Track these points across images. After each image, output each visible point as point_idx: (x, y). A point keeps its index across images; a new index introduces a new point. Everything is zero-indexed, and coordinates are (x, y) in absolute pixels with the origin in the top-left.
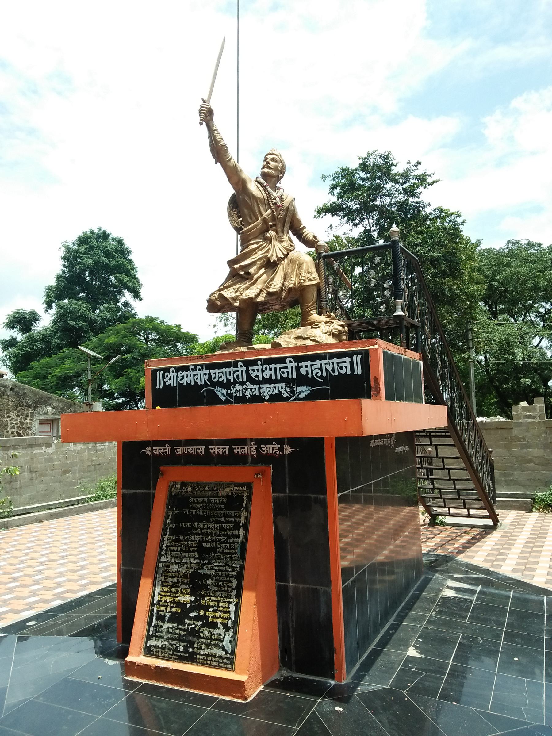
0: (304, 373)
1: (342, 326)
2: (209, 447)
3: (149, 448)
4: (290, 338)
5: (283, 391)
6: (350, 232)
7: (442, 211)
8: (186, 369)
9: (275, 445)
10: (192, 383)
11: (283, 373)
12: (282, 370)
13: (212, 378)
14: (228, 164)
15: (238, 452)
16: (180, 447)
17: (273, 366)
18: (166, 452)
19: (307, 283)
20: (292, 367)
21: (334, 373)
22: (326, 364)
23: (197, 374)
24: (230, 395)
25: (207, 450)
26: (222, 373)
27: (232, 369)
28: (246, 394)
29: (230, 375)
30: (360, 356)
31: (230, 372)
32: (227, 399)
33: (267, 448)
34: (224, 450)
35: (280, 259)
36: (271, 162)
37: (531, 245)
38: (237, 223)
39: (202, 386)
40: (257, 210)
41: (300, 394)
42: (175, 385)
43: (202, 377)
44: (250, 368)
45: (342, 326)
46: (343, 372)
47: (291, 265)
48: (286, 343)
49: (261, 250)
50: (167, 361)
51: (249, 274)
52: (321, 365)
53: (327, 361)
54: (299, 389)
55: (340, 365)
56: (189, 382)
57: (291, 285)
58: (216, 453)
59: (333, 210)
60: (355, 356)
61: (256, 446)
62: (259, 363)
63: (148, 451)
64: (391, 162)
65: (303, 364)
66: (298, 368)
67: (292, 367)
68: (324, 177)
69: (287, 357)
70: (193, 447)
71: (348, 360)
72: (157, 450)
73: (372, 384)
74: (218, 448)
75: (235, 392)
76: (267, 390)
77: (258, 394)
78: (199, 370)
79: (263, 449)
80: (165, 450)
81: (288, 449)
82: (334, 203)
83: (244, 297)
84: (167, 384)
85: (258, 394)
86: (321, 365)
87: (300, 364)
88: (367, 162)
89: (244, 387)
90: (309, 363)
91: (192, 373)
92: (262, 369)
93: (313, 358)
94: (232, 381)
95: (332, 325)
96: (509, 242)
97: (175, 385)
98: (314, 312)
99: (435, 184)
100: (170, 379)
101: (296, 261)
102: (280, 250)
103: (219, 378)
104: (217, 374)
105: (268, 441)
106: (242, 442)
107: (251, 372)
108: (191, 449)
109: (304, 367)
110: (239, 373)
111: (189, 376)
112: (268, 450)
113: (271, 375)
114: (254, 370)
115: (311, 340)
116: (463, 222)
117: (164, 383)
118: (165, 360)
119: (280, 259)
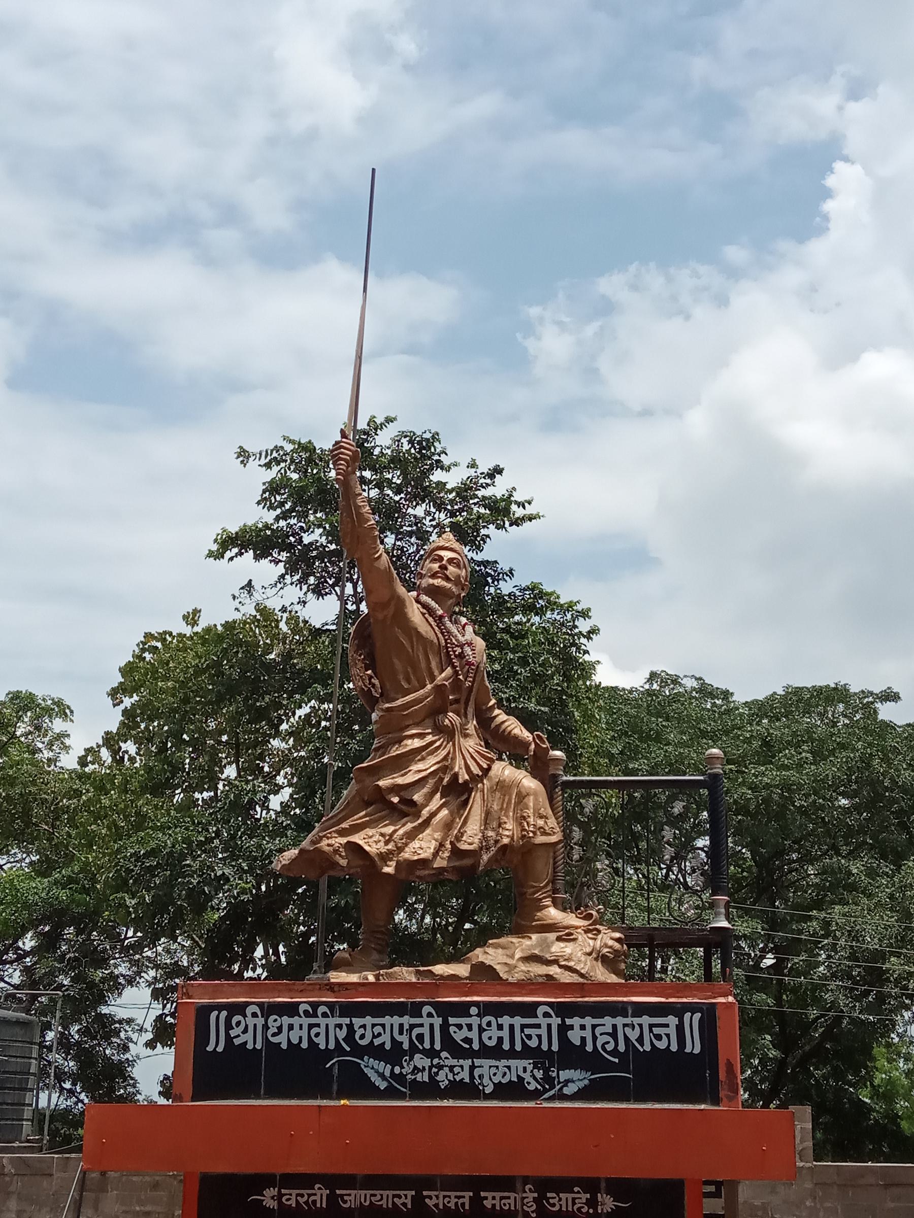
0: (577, 1042)
1: (618, 940)
2: (425, 1193)
3: (271, 1192)
4: (512, 956)
5: (527, 1077)
6: (298, 607)
7: (542, 595)
8: (291, 1010)
9: (578, 1192)
10: (304, 1045)
11: (529, 1037)
12: (527, 1031)
13: (357, 1037)
14: (376, 564)
15: (494, 1205)
16: (353, 1192)
17: (506, 1020)
18: (314, 1202)
19: (540, 839)
20: (549, 1026)
21: (642, 1045)
22: (625, 1025)
23: (318, 1025)
24: (400, 1078)
25: (418, 1200)
26: (383, 1026)
27: (407, 1020)
28: (438, 1078)
29: (401, 1033)
30: (698, 1016)
31: (401, 1026)
32: (390, 1087)
33: (560, 1200)
34: (461, 1201)
35: (476, 779)
36: (450, 568)
37: (706, 691)
38: (363, 680)
39: (328, 1054)
40: (423, 665)
41: (566, 1085)
42: (258, 1046)
43: (329, 1032)
44: (452, 1020)
45: (618, 940)
46: (662, 1045)
47: (498, 794)
48: (507, 969)
49: (432, 753)
50: (238, 989)
51: (413, 803)
52: (614, 1027)
53: (628, 1020)
54: (564, 1075)
55: (656, 1030)
56: (295, 1041)
57: (506, 841)
58: (441, 1207)
59: (257, 541)
60: (687, 1015)
61: (536, 1195)
62: (474, 1010)
63: (269, 1198)
64: (436, 457)
65: (576, 1021)
66: (564, 1029)
67: (549, 1026)
68: (243, 455)
69: (539, 1004)
70: (385, 1193)
71: (672, 1020)
72: (291, 1197)
73: (722, 1075)
74: (445, 1197)
75: (413, 1073)
76: (490, 1073)
77: (467, 1080)
78: (325, 1015)
79: (551, 1201)
80: (312, 1198)
81: (607, 1203)
82: (267, 526)
83: (407, 855)
84: (237, 1042)
85: (467, 1080)
86: (614, 1027)
87: (568, 1021)
88: (366, 441)
89: (436, 1061)
90: (588, 1021)
91: (306, 1021)
92: (480, 1026)
93: (598, 1010)
94: (406, 1046)
95: (600, 937)
96: (653, 676)
97: (258, 1046)
98: (548, 902)
99: (527, 524)
100: (245, 1031)
101: (510, 787)
102: (472, 757)
103: (374, 1037)
104: (369, 1028)
105: (563, 1185)
106: (504, 1183)
107: (452, 1029)
108: (379, 1197)
109: (577, 1027)
110: (426, 1031)
111: (296, 1027)
112: (563, 1203)
113: (500, 1039)
114: (460, 1027)
115: (561, 967)
116: (594, 631)
117: (229, 1039)
118: (233, 985)
119: (476, 779)
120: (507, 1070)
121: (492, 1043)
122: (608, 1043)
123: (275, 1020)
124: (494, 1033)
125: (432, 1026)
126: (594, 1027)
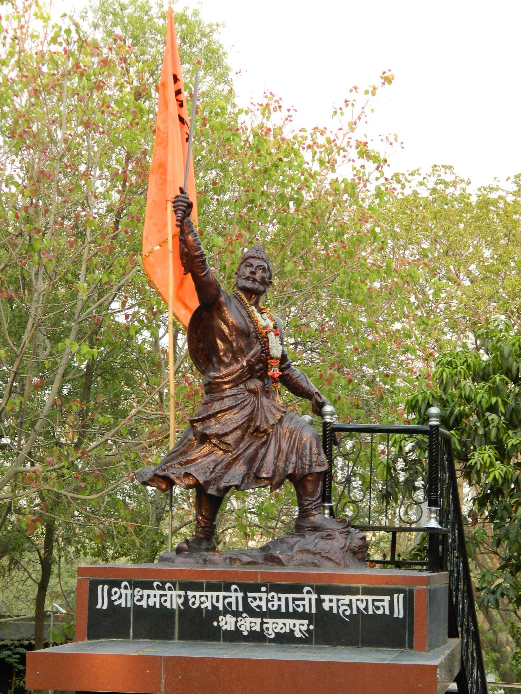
10: (158, 606)
22: (357, 600)
23: (166, 595)
27: (221, 594)
29: (218, 601)
31: (218, 597)
44: (250, 594)
52: (351, 601)
55: (377, 604)
60: (396, 596)
65: (327, 597)
66: (319, 602)
71: (387, 598)
76: (274, 626)
78: (170, 589)
84: (116, 603)
86: (351, 601)
87: (322, 597)
91: (158, 593)
92: (267, 598)
100: (120, 598)
107: (249, 600)
109: (327, 600)
113: (280, 606)
114: (255, 599)
120: (283, 626)
121: (275, 608)
122: (346, 610)
123: (139, 592)
124: (276, 603)
125: (237, 598)
126: (338, 600)
